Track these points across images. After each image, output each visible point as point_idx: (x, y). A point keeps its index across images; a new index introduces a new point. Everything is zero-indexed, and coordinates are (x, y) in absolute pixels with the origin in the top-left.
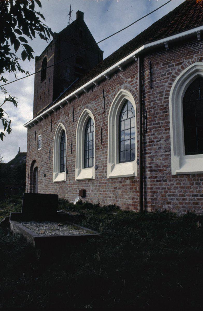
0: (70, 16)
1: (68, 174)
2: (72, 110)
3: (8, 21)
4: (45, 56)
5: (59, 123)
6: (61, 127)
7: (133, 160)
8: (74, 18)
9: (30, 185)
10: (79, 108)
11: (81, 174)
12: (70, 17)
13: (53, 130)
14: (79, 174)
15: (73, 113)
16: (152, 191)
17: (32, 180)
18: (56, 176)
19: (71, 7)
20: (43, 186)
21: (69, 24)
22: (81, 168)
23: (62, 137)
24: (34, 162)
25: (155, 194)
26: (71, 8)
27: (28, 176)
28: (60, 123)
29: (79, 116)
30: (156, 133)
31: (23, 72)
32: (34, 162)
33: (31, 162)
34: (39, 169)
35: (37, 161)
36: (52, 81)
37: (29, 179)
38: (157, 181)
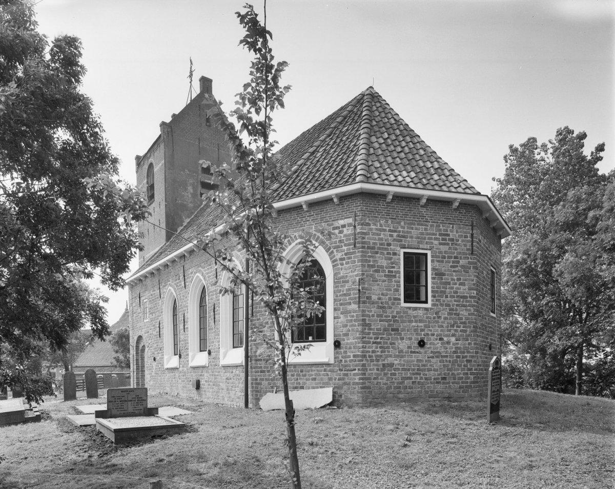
0: (191, 80)
1: (182, 360)
2: (182, 271)
3: (4, 254)
4: (150, 160)
5: (168, 287)
6: (172, 293)
7: (242, 347)
8: (197, 90)
9: (137, 371)
10: (190, 270)
11: (226, 358)
12: (191, 82)
13: (162, 296)
14: (224, 357)
15: (184, 276)
16: (257, 383)
17: (138, 364)
18: (170, 359)
19: (193, 62)
20: (153, 374)
21: (189, 102)
22: (228, 348)
23: (174, 306)
24: (140, 338)
25: (259, 386)
26: (191, 63)
27: (134, 358)
28: (170, 288)
29: (191, 282)
30: (261, 318)
31: (241, 23)
32: (140, 338)
33: (136, 338)
34: (147, 349)
35: (144, 337)
36: (163, 207)
37: (135, 364)
38: (261, 372)
